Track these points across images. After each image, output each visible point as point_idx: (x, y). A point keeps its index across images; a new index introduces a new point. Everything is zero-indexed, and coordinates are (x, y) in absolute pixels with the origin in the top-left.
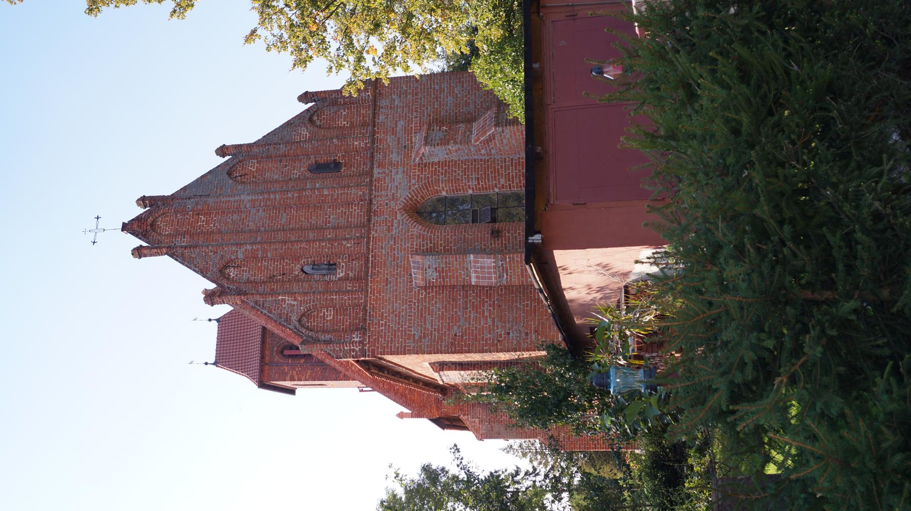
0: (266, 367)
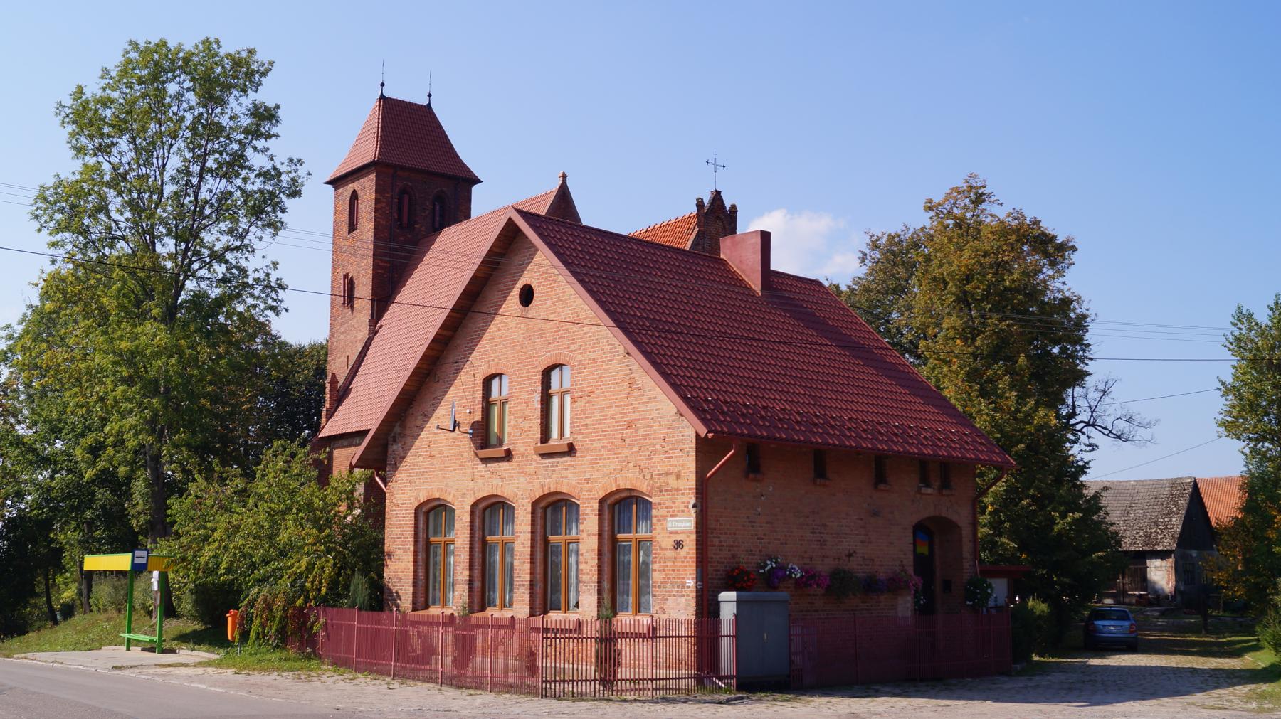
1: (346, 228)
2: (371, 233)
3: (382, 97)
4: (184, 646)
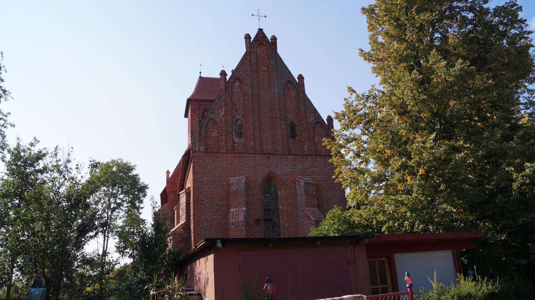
0: (198, 103)
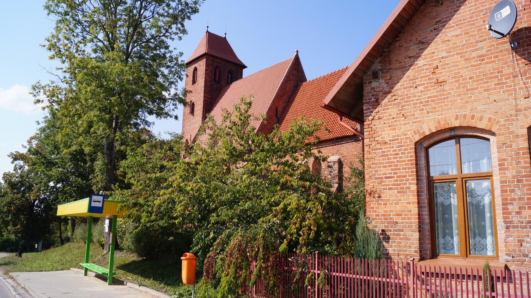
0: (212, 58)
1: (191, 83)
2: (203, 83)
3: (207, 32)
4: (130, 276)
